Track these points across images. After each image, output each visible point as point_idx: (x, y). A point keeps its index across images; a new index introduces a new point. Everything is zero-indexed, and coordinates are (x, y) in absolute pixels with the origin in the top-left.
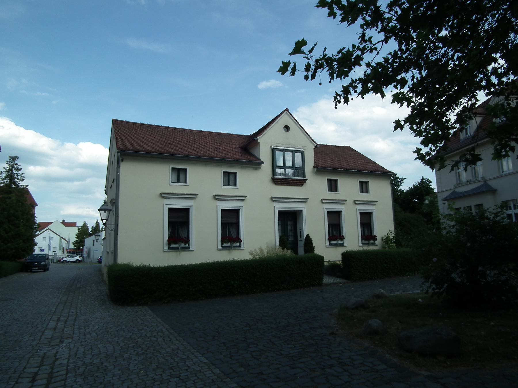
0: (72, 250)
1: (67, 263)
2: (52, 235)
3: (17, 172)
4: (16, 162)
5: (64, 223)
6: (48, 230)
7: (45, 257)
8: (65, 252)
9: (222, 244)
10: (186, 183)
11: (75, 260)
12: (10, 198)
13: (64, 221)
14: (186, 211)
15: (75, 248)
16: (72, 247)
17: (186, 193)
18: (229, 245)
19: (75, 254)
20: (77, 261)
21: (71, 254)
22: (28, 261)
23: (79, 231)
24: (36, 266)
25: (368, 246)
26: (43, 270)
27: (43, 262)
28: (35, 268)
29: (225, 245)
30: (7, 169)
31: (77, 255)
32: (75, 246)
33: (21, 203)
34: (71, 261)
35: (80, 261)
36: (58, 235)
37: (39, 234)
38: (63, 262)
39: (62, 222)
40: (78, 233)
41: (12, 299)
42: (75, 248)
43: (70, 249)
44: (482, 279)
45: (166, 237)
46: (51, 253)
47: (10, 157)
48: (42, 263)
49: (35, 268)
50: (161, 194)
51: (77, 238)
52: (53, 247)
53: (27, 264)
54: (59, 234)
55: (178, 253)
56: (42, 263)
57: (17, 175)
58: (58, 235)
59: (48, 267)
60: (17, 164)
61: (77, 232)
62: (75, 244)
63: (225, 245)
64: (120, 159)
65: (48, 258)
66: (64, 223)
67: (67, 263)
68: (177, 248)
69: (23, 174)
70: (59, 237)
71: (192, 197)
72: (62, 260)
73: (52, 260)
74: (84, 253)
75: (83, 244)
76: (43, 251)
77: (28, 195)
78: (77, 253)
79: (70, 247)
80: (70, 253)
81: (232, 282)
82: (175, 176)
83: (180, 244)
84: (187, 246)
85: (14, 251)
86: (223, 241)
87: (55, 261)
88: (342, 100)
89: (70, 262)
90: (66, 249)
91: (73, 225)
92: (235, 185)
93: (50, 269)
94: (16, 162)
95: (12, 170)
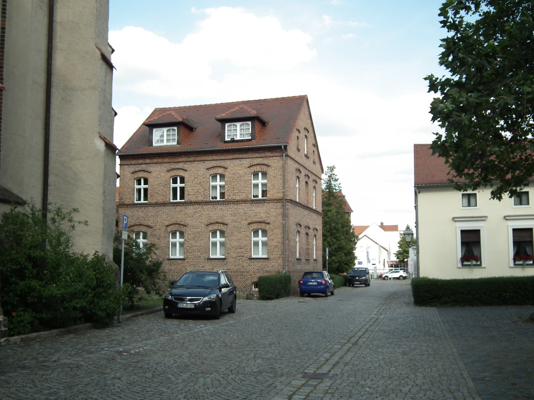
0: (395, 263)
1: (389, 280)
3: (334, 183)
4: (334, 172)
5: (382, 226)
7: (365, 272)
8: (387, 266)
9: (515, 262)
10: (476, 206)
11: (398, 276)
12: (331, 211)
13: (382, 224)
14: (477, 232)
15: (398, 260)
16: (394, 259)
17: (475, 215)
18: (521, 262)
19: (399, 269)
20: (401, 278)
21: (394, 269)
22: (350, 275)
23: (401, 238)
24: (357, 281)
25: (522, 268)
26: (364, 285)
27: (364, 276)
28: (356, 283)
29: (517, 263)
30: (326, 180)
31: (401, 269)
32: (398, 258)
33: (340, 216)
34: (393, 278)
35: (405, 278)
38: (384, 279)
40: (401, 241)
42: (398, 260)
43: (392, 261)
45: (460, 256)
46: (370, 267)
47: (328, 167)
48: (363, 278)
49: (356, 283)
50: (453, 218)
51: (400, 247)
53: (350, 278)
55: (471, 269)
56: (363, 278)
57: (335, 186)
58: (376, 243)
59: (368, 282)
60: (334, 174)
61: (399, 239)
62: (398, 255)
63: (517, 263)
64: (417, 191)
65: (368, 273)
66: (382, 226)
67: (389, 280)
68: (470, 265)
69: (340, 184)
71: (482, 219)
72: (383, 276)
73: (371, 275)
74: (409, 267)
75: (407, 255)
76: (361, 264)
77: (345, 206)
78: (400, 266)
79: (392, 260)
80: (392, 267)
81: (504, 294)
82: (466, 201)
83: (472, 262)
84: (479, 263)
85: (338, 264)
86: (515, 260)
87: (375, 277)
89: (392, 279)
90: (388, 262)
91: (394, 228)
92: (528, 204)
93: (370, 285)
94: (334, 172)
95: (330, 181)
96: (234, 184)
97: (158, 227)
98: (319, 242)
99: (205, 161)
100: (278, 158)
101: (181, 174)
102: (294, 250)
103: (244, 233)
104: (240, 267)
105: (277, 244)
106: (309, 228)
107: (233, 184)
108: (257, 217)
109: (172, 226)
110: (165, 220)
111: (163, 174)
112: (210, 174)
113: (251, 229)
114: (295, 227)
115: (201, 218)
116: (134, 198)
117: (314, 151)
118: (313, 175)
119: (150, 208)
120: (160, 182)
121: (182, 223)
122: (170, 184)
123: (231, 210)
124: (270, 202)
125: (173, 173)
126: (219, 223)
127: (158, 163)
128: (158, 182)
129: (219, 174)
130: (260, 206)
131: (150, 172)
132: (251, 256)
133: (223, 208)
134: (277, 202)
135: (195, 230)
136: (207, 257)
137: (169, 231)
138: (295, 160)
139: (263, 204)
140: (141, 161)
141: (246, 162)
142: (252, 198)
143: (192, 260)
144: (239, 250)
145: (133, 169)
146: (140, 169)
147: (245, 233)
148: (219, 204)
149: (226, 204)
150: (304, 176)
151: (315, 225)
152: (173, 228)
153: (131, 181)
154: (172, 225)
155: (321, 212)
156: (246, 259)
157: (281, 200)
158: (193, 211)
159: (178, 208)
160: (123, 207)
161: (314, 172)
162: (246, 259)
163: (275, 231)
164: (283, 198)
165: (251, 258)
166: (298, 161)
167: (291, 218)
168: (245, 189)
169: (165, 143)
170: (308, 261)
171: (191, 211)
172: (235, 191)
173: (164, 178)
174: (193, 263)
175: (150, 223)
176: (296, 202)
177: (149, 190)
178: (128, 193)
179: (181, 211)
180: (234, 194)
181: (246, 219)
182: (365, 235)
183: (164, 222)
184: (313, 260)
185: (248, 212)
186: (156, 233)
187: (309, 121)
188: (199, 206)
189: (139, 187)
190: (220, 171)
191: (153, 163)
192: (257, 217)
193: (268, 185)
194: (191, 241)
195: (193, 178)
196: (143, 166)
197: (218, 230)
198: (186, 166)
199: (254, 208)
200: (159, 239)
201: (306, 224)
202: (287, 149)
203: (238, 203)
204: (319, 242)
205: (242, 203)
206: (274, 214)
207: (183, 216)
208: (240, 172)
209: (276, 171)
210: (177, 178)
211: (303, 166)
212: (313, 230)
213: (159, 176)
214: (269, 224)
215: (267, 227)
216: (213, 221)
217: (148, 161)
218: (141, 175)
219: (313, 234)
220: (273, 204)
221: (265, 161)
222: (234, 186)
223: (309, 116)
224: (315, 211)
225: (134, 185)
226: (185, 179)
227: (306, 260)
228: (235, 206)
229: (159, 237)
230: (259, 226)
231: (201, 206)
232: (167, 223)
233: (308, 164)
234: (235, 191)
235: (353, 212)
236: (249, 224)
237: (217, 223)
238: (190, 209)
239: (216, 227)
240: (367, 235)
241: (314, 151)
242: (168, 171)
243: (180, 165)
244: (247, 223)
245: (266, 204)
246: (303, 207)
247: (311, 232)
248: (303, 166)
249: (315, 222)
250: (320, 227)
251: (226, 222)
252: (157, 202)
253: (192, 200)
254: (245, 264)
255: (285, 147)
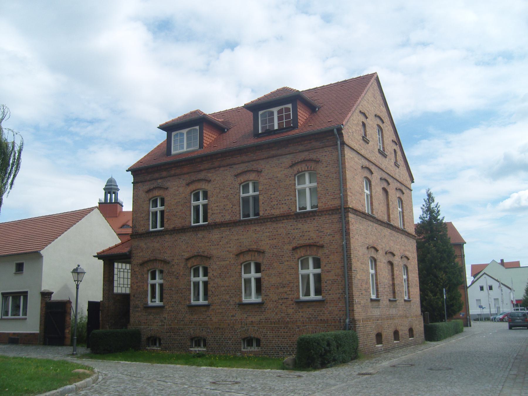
2: (491, 282)
5: (502, 262)
6: (485, 275)
20: (497, 306)
21: (519, 308)
36: (497, 281)
37: (474, 280)
39: (500, 262)
41: (450, 369)
44: (149, 347)
52: (476, 300)
54: (499, 280)
58: (497, 281)
70: (498, 283)
88: (423, 207)
96: (271, 193)
97: (177, 261)
98: (413, 275)
99: (232, 165)
100: (330, 149)
101: (203, 187)
102: (364, 286)
103: (286, 263)
104: (283, 315)
105: (336, 278)
106: (394, 255)
107: (270, 193)
108: (305, 238)
109: (193, 260)
110: (184, 252)
111: (181, 189)
112: (239, 182)
113: (297, 256)
114: (366, 251)
115: (229, 245)
116: (149, 224)
117: (395, 151)
118: (395, 181)
119: (167, 236)
120: (178, 200)
121: (206, 254)
122: (190, 202)
123: (268, 230)
124: (322, 215)
125: (193, 187)
126: (253, 251)
127: (175, 176)
128: (176, 201)
129: (251, 180)
130: (308, 221)
131: (167, 189)
132: (299, 298)
133: (258, 228)
134: (332, 214)
135: (222, 263)
136: (238, 302)
137: (189, 267)
138: (358, 153)
139: (312, 218)
140: (156, 175)
141: (287, 160)
142: (298, 211)
143: (218, 307)
144: (281, 290)
145: (146, 187)
146: (155, 185)
147: (289, 263)
148: (251, 224)
149: (261, 223)
150: (379, 180)
151: (404, 251)
152: (194, 262)
153: (145, 203)
154: (193, 257)
155: (414, 234)
156: (291, 302)
157: (338, 209)
158: (219, 236)
159: (200, 235)
160: (137, 238)
161: (398, 178)
162: (291, 302)
163: (331, 257)
164: (341, 206)
165: (298, 300)
166: (367, 156)
167: (357, 237)
168: (286, 198)
169: (185, 150)
170: (394, 303)
171: (216, 236)
172: (273, 203)
173: (183, 195)
174: (220, 311)
175: (167, 257)
176: (363, 213)
177: (165, 212)
178: (142, 219)
179: (203, 237)
180: (272, 208)
181: (290, 243)
182: (485, 273)
183: (183, 254)
184: (403, 301)
185: (292, 231)
186: (173, 270)
187: (384, 109)
188: (226, 228)
189: (154, 209)
190: (252, 176)
191: (170, 176)
192: (305, 238)
193: (318, 189)
194: (216, 280)
195: (218, 191)
196: (159, 181)
197: (251, 260)
198: (209, 175)
199: (300, 226)
200: (177, 278)
201: (388, 249)
202: (342, 134)
203: (277, 220)
204: (413, 275)
205: (284, 220)
206: (329, 231)
207: (207, 244)
208: (279, 175)
209: (328, 168)
210: (199, 192)
211: (376, 166)
212: (402, 258)
213: (177, 192)
214: (322, 246)
215: (320, 254)
216: (244, 249)
217: (164, 174)
218: (156, 193)
219: (402, 264)
220: (327, 216)
221: (313, 156)
222: (272, 196)
223: (382, 102)
224: (408, 234)
225: (149, 207)
226: (208, 193)
227: (390, 300)
228: (275, 225)
229: (177, 275)
230: (308, 251)
231: (229, 228)
232: (187, 255)
233: (387, 164)
234: (273, 203)
235: (465, 243)
236: (295, 249)
237: (249, 251)
238: (215, 235)
239: (248, 257)
240: (486, 273)
241: (395, 151)
242: (188, 185)
243: (202, 175)
244: (290, 248)
245: (317, 217)
246: (379, 223)
247: (396, 260)
248: (376, 166)
249: (403, 247)
250: (413, 255)
251: (262, 248)
252: (174, 228)
253: (217, 220)
254: (290, 311)
255: (340, 130)
